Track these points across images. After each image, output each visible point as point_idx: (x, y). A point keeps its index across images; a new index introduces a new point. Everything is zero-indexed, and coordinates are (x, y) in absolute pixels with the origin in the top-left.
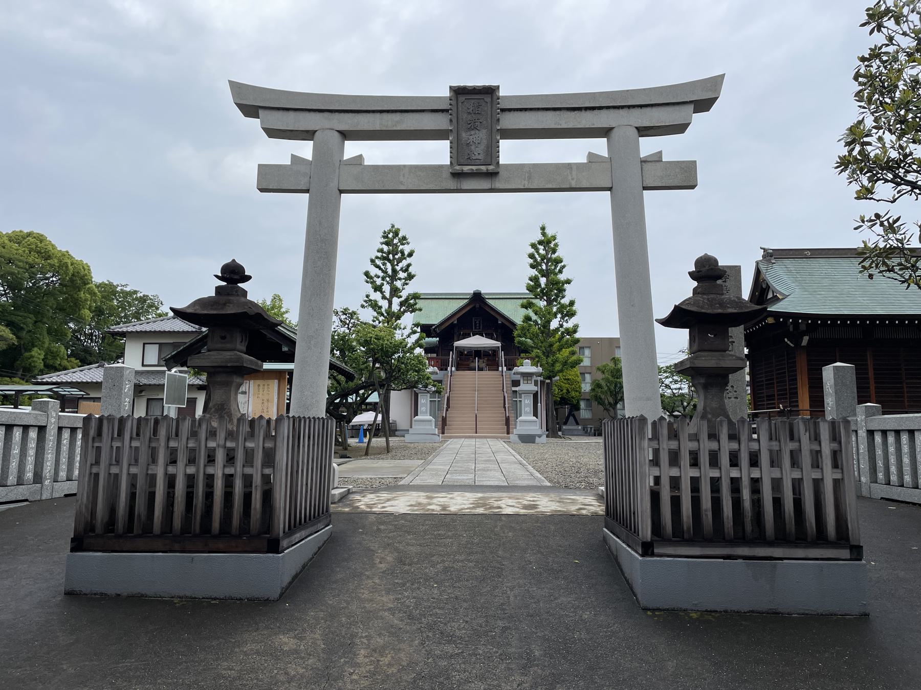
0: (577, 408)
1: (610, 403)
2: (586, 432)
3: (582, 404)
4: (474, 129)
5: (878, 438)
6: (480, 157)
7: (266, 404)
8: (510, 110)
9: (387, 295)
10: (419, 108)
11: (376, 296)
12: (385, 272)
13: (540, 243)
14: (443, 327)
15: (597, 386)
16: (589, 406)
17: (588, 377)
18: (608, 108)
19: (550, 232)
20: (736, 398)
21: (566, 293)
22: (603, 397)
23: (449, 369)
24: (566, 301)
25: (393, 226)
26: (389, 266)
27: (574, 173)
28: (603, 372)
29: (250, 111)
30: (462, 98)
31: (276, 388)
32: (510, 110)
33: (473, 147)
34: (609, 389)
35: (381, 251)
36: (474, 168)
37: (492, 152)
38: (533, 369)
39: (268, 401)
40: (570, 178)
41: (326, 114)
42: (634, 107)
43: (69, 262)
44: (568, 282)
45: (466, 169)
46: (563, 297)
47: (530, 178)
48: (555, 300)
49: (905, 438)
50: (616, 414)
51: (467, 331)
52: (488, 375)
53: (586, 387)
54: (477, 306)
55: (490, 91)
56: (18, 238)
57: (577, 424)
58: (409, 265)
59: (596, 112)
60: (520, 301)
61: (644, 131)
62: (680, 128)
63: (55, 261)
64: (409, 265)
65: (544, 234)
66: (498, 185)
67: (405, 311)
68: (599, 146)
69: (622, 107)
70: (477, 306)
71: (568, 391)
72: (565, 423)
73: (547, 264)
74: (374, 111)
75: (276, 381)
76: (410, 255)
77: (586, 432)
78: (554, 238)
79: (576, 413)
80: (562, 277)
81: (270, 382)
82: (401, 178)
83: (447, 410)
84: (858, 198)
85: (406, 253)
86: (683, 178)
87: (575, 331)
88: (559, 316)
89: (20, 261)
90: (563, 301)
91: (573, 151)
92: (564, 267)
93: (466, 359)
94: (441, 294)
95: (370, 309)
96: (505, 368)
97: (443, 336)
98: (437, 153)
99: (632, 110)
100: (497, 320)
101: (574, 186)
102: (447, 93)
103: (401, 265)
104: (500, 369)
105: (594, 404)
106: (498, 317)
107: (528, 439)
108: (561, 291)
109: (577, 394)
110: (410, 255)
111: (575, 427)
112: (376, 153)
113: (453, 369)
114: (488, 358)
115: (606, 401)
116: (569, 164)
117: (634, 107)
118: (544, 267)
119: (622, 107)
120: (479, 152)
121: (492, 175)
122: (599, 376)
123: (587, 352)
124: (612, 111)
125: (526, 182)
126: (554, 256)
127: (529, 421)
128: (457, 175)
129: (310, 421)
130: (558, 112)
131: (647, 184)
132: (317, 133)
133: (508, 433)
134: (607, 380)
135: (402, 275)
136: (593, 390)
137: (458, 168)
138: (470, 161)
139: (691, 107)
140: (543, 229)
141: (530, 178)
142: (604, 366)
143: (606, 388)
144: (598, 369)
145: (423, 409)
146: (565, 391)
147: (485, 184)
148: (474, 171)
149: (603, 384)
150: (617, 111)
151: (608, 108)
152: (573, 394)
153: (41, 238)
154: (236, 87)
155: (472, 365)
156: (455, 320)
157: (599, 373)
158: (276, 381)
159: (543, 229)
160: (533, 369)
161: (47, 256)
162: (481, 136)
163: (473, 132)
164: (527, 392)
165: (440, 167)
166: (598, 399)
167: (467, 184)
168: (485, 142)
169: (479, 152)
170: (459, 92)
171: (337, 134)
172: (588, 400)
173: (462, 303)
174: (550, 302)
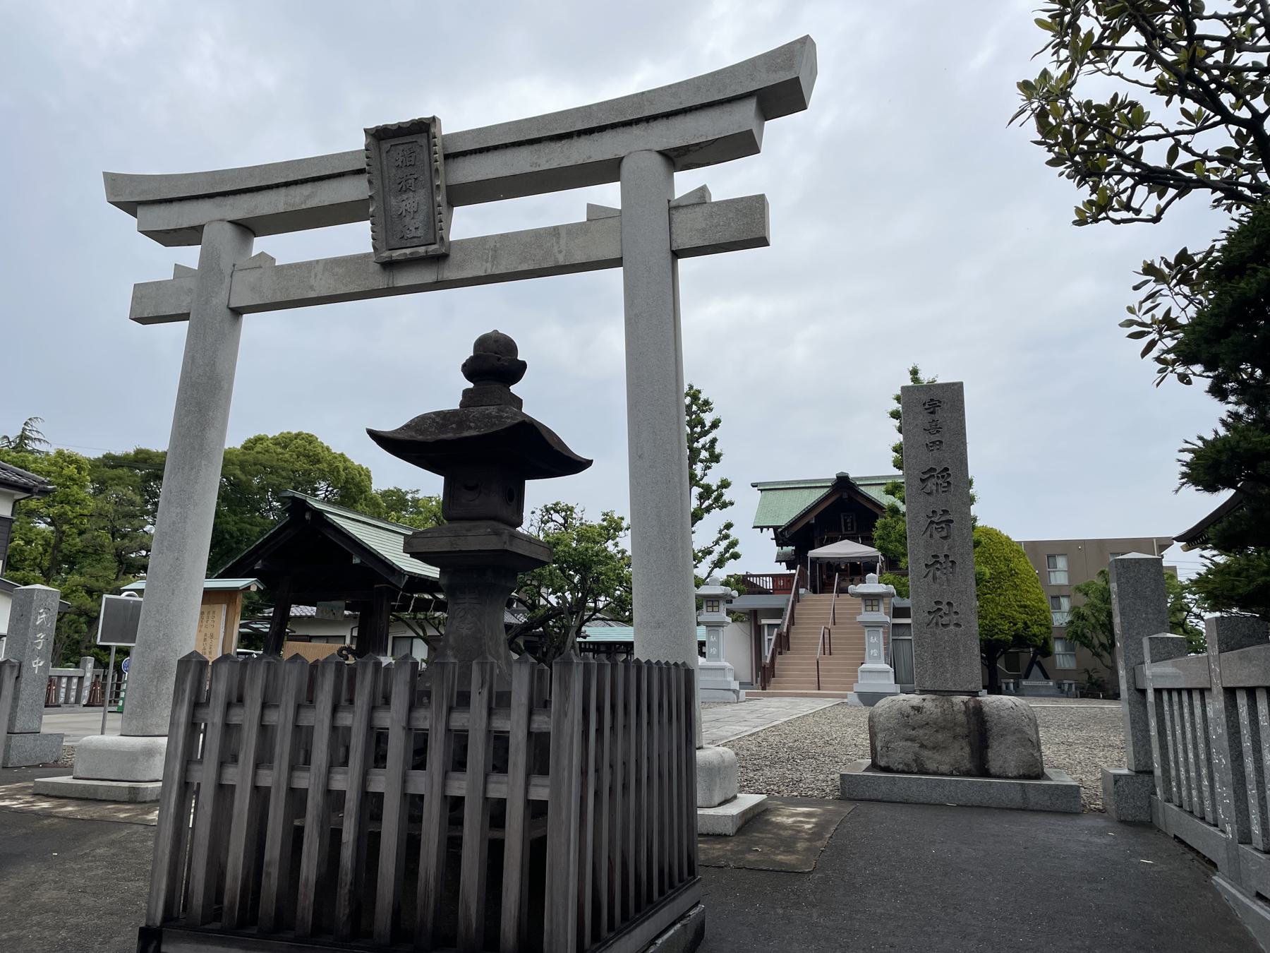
0: (1045, 650)
1: (1102, 645)
2: (1062, 691)
3: (1058, 647)
4: (408, 192)
5: (1242, 701)
6: (419, 234)
7: (209, 640)
8: (464, 154)
10: (336, 171)
15: (1078, 616)
16: (1069, 649)
17: (1065, 604)
18: (614, 126)
20: (957, 625)
27: (563, 242)
28: (1086, 594)
29: (130, 207)
30: (386, 145)
31: (224, 612)
32: (464, 154)
33: (407, 220)
34: (1098, 620)
36: (408, 251)
37: (436, 225)
39: (212, 636)
40: (556, 249)
41: (218, 200)
42: (655, 118)
43: (341, 466)
45: (396, 254)
47: (495, 258)
49: (1196, 696)
51: (832, 535)
53: (1060, 618)
54: (845, 496)
55: (424, 128)
56: (285, 442)
57: (1047, 677)
58: (714, 441)
59: (596, 136)
60: (883, 488)
61: (678, 158)
62: (745, 145)
63: (324, 466)
64: (714, 441)
66: (449, 274)
67: (708, 510)
68: (609, 195)
69: (637, 122)
70: (845, 496)
71: (1026, 626)
72: (1027, 677)
74: (278, 186)
75: (224, 606)
76: (715, 425)
77: (1062, 691)
79: (1046, 662)
81: (216, 607)
82: (312, 281)
84: (1081, 222)
85: (708, 424)
86: (745, 228)
89: (284, 469)
91: (566, 207)
94: (799, 482)
98: (355, 239)
99: (653, 124)
101: (562, 260)
102: (360, 143)
103: (702, 441)
109: (1043, 629)
110: (715, 425)
111: (1044, 683)
112: (285, 248)
115: (1096, 642)
116: (556, 228)
117: (655, 118)
119: (637, 122)
120: (416, 226)
121: (440, 259)
122: (1081, 600)
123: (1061, 563)
124: (620, 130)
125: (489, 265)
128: (389, 266)
129: (661, 669)
130: (536, 147)
131: (682, 242)
132: (214, 230)
134: (1093, 606)
135: (704, 454)
137: (386, 254)
138: (404, 242)
139: (751, 106)
140: (914, 372)
141: (495, 258)
142: (1088, 585)
143: (1093, 621)
144: (1078, 589)
145: (874, 652)
146: (1020, 625)
147: (428, 276)
148: (411, 260)
149: (1086, 612)
150: (628, 130)
151: (614, 126)
152: (1035, 629)
153: (310, 439)
154: (113, 182)
156: (811, 519)
158: (224, 606)
159: (914, 372)
161: (315, 459)
162: (416, 200)
163: (405, 197)
165: (366, 256)
166: (1084, 641)
167: (404, 279)
168: (423, 208)
169: (416, 226)
170: (379, 136)
171: (228, 226)
173: (820, 493)
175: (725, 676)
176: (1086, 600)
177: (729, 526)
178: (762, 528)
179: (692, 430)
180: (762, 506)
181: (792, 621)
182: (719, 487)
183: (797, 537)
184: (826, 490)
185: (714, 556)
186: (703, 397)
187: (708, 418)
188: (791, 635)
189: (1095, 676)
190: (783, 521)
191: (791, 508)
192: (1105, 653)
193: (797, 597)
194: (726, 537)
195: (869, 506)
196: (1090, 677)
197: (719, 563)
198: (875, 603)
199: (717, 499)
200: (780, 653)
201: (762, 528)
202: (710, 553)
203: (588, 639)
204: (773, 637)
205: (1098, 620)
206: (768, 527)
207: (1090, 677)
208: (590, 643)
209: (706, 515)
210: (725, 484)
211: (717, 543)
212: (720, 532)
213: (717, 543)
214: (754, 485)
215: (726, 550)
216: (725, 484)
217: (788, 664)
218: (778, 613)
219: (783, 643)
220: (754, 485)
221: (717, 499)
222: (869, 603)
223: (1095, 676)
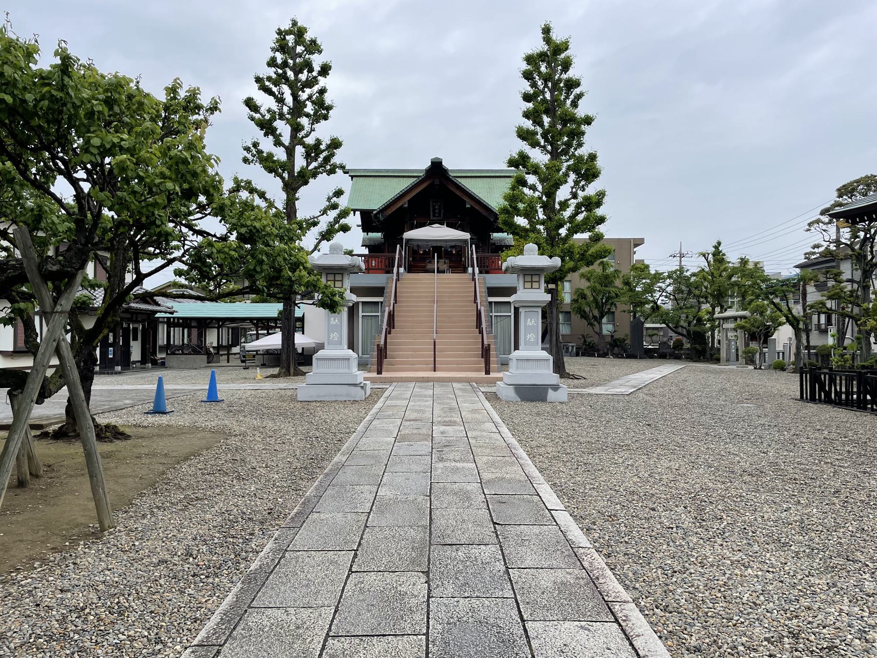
1: (594, 317)
9: (286, 140)
11: (267, 145)
12: (281, 100)
13: (542, 56)
14: (389, 212)
19: (557, 36)
21: (585, 139)
22: (587, 309)
23: (395, 269)
24: (584, 151)
25: (295, 23)
26: (286, 89)
28: (588, 280)
35: (272, 63)
38: (544, 261)
44: (588, 121)
46: (580, 145)
48: (565, 152)
50: (601, 329)
52: (451, 277)
54: (437, 182)
64: (322, 91)
65: (548, 40)
67: (314, 174)
70: (437, 182)
73: (552, 91)
78: (565, 46)
80: (581, 112)
83: (388, 332)
85: (317, 68)
87: (599, 204)
88: (572, 176)
90: (579, 152)
92: (579, 96)
93: (421, 259)
95: (258, 166)
96: (477, 270)
97: (387, 226)
100: (464, 202)
104: (470, 270)
105: (576, 317)
106: (466, 198)
107: (532, 394)
108: (577, 135)
110: (325, 70)
113: (402, 270)
114: (452, 258)
118: (548, 96)
126: (564, 76)
127: (531, 360)
133: (488, 372)
135: (309, 108)
136: (574, 301)
140: (547, 31)
149: (588, 293)
155: (429, 266)
156: (404, 203)
157: (583, 281)
159: (547, 31)
160: (544, 261)
164: (530, 305)
172: (566, 313)
174: (555, 155)
175: (349, 367)
176: (588, 284)
177: (339, 193)
179: (296, 75)
182: (329, 147)
184: (413, 180)
185: (323, 226)
186: (308, 37)
187: (317, 61)
189: (588, 340)
192: (596, 323)
194: (334, 207)
195: (458, 193)
196: (585, 341)
197: (327, 236)
199: (327, 159)
202: (315, 224)
203: (175, 315)
206: (357, 210)
207: (585, 341)
208: (179, 318)
209: (311, 180)
210: (335, 144)
211: (324, 212)
212: (329, 199)
213: (324, 212)
215: (336, 220)
216: (335, 144)
221: (327, 159)
222: (528, 278)
223: (588, 340)
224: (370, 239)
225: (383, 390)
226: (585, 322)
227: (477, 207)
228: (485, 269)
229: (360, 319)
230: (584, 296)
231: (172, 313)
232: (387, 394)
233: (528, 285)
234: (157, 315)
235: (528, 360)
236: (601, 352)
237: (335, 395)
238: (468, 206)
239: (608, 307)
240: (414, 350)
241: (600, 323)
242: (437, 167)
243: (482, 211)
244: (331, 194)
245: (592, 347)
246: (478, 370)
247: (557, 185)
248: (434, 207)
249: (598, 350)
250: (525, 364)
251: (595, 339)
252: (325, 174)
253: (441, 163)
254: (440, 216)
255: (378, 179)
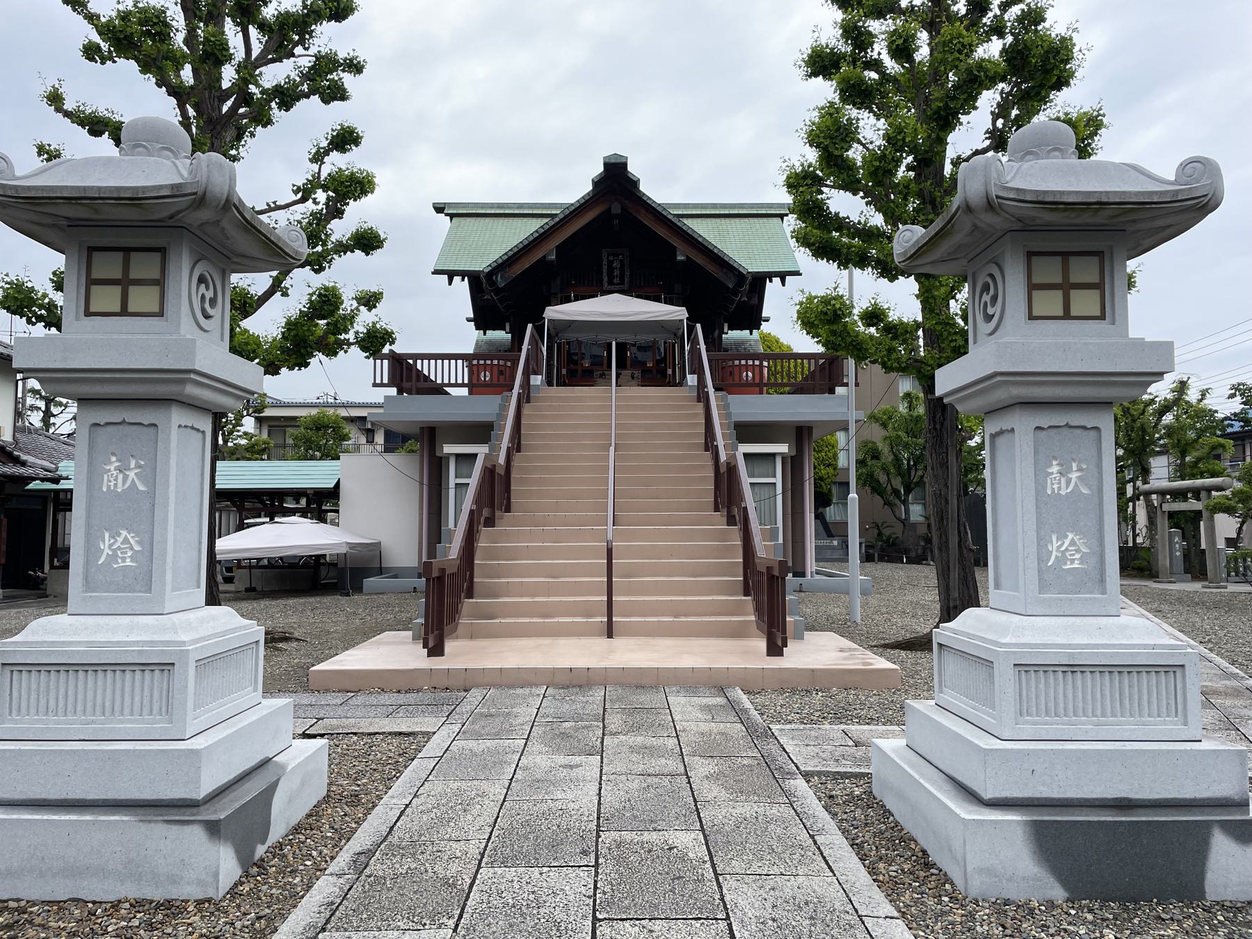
14: (518, 269)
22: (883, 478)
28: (884, 425)
50: (907, 512)
54: (616, 209)
70: (616, 209)
93: (578, 361)
100: (673, 250)
104: (692, 379)
106: (674, 241)
114: (649, 361)
133: (775, 649)
156: (549, 251)
176: (885, 433)
178: (451, 275)
180: (451, 239)
181: (517, 443)
183: (505, 297)
188: (514, 475)
189: (886, 532)
190: (481, 264)
191: (492, 245)
193: (526, 396)
196: (880, 534)
198: (144, 266)
200: (490, 522)
201: (451, 275)
204: (473, 481)
205: (897, 460)
206: (463, 274)
207: (880, 534)
214: (439, 209)
217: (513, 554)
218: (481, 432)
219: (496, 494)
220: (439, 209)
222: (1049, 271)
223: (886, 532)
224: (490, 343)
225: (412, 742)
226: (878, 500)
227: (700, 260)
228: (728, 382)
229: (452, 492)
230: (876, 455)
231: (56, 480)
232: (433, 748)
233: (1050, 302)
234: (31, 486)
235: (1072, 668)
236: (913, 554)
237: (73, 872)
238: (680, 258)
239: (920, 473)
240: (553, 572)
241: (905, 502)
242: (616, 179)
243: (711, 268)
244: (324, 144)
245: (894, 544)
246: (737, 632)
247: (945, 120)
248: (610, 263)
249: (906, 552)
250: (1059, 685)
251: (898, 530)
252: (315, 99)
253: (625, 165)
254: (622, 283)
255: (501, 220)
